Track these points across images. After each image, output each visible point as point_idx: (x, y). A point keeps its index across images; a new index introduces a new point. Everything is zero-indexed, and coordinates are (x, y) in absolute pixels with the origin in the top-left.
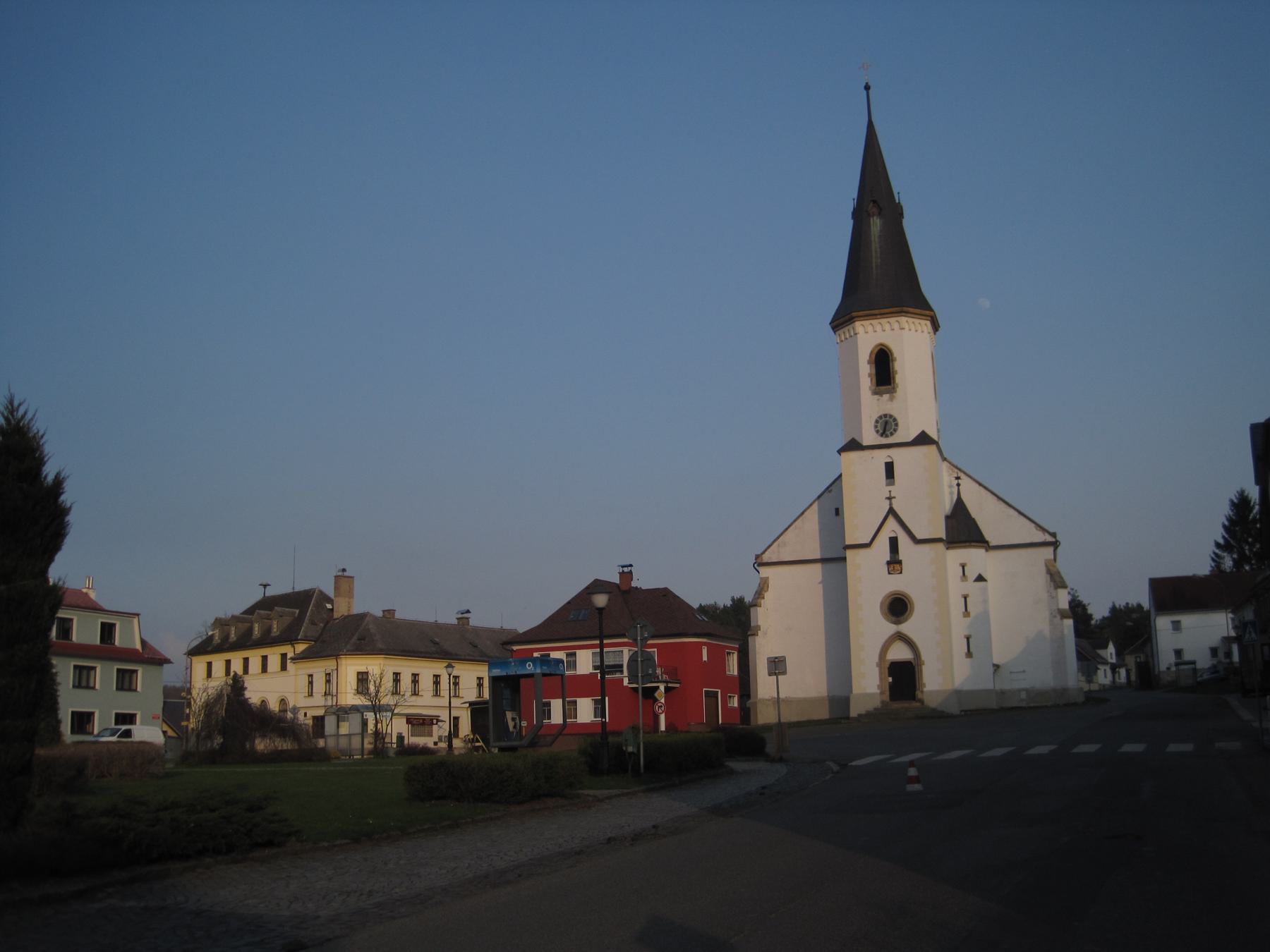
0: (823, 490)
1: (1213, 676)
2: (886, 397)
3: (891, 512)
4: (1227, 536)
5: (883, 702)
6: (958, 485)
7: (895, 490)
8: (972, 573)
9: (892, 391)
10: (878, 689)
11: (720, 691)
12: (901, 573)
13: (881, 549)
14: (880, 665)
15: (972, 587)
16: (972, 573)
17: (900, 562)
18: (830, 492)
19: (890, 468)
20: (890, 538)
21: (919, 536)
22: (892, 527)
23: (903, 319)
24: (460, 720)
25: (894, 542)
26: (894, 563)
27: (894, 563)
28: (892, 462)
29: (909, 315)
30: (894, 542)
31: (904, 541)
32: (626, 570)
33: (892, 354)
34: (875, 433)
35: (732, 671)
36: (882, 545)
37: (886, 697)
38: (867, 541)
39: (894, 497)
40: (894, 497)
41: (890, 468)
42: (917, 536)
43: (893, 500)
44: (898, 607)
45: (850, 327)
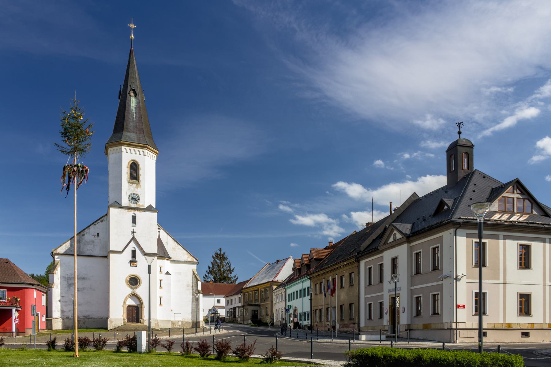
1: (396, 310)
2: (134, 185)
3: (133, 239)
6: (159, 232)
8: (164, 271)
11: (40, 313)
12: (136, 266)
13: (127, 254)
15: (163, 276)
16: (164, 271)
17: (136, 262)
20: (132, 250)
23: (146, 151)
24: (388, 292)
25: (134, 252)
26: (133, 261)
27: (133, 261)
30: (134, 252)
31: (138, 252)
36: (128, 252)
37: (126, 321)
38: (121, 250)
39: (136, 232)
40: (136, 232)
43: (135, 233)
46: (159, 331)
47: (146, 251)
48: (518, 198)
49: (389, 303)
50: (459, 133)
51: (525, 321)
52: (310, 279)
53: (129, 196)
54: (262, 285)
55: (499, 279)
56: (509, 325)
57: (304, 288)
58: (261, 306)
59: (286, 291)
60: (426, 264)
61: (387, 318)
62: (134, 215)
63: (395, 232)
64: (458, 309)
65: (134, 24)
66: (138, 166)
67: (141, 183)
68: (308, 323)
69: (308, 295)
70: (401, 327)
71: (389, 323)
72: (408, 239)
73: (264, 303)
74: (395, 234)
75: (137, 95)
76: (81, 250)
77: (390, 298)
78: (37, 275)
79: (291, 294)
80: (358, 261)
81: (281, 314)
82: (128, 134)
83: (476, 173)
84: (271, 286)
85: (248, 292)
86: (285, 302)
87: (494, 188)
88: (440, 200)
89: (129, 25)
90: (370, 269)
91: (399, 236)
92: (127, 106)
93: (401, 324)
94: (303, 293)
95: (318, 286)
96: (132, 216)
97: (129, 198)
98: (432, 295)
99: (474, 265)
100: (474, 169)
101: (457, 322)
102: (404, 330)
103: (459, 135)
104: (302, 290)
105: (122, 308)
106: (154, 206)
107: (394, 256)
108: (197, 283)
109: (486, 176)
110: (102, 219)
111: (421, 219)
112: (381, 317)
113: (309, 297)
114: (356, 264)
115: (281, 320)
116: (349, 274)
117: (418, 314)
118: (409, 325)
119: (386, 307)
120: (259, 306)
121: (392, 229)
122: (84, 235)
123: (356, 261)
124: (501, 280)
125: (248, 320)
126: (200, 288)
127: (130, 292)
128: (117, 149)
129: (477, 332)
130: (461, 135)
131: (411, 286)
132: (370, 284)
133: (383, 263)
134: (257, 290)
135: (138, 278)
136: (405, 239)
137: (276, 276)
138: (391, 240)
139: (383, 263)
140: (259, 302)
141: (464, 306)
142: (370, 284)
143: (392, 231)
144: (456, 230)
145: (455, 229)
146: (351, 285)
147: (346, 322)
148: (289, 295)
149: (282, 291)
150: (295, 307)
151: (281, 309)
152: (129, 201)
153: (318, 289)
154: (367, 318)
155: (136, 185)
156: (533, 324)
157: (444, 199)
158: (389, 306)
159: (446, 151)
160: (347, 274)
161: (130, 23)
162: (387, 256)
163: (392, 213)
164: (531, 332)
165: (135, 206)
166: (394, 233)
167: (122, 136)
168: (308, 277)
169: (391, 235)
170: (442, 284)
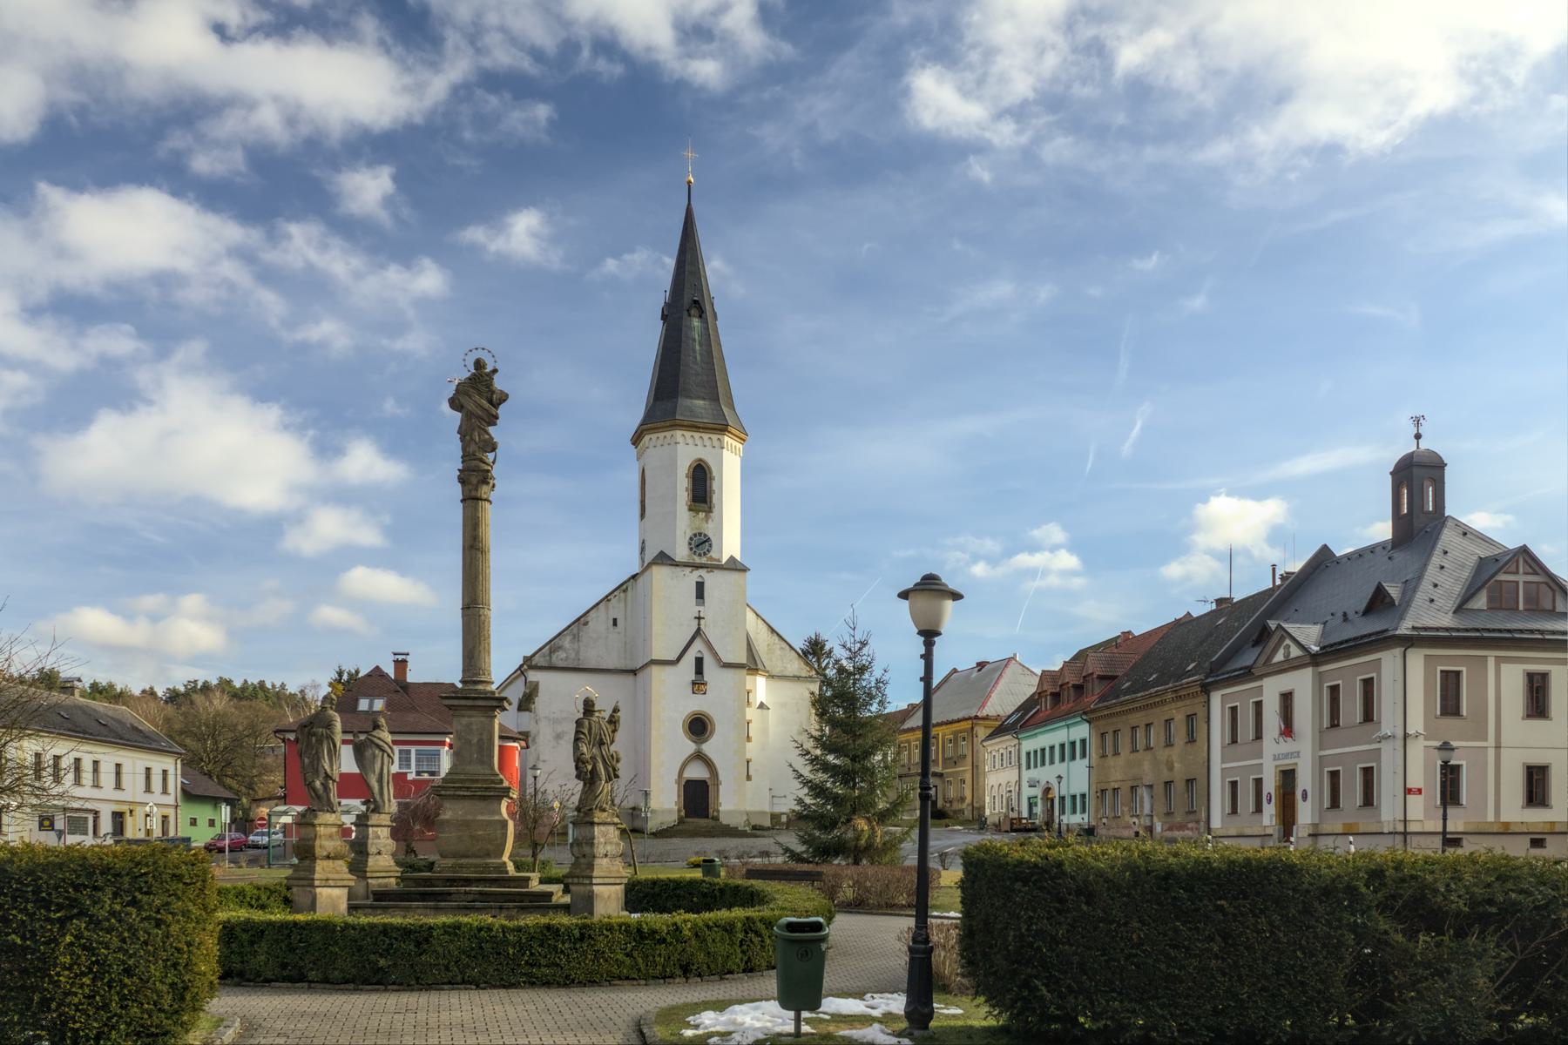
0: (601, 598)
2: (702, 515)
3: (698, 632)
4: (480, 687)
10: (676, 805)
12: (705, 693)
14: (678, 782)
18: (608, 600)
19: (700, 587)
20: (696, 658)
21: (673, 657)
25: (699, 662)
26: (698, 685)
27: (698, 685)
28: (703, 583)
29: (1477, 534)
30: (699, 662)
32: (400, 658)
33: (711, 472)
34: (688, 550)
35: (179, 762)
36: (690, 659)
37: (683, 814)
39: (703, 618)
40: (703, 618)
41: (700, 587)
42: (672, 659)
44: (699, 727)
46: (743, 834)
47: (726, 659)
48: (1525, 582)
49: (1276, 782)
50: (1418, 436)
51: (1536, 816)
52: (1089, 722)
53: (691, 539)
54: (948, 726)
55: (1486, 740)
56: (1507, 824)
57: (1072, 739)
58: (945, 775)
59: (1020, 744)
60: (1351, 708)
61: (1270, 811)
62: (700, 580)
63: (1288, 641)
64: (1408, 796)
66: (708, 472)
67: (714, 510)
68: (1083, 819)
69: (1083, 755)
70: (1300, 829)
71: (1274, 818)
72: (1314, 660)
73: (954, 770)
74: (1288, 647)
75: (703, 312)
76: (581, 658)
77: (1278, 771)
78: (273, 686)
79: (1036, 752)
80: (1206, 689)
81: (1004, 797)
82: (688, 402)
83: (1449, 524)
84: (972, 728)
85: (908, 742)
86: (1017, 770)
87: (1482, 556)
88: (1376, 583)
90: (1234, 710)
91: (1295, 652)
92: (683, 339)
93: (1299, 822)
94: (1069, 752)
95: (1109, 738)
96: (697, 583)
97: (690, 544)
98: (1360, 768)
99: (1439, 713)
100: (1446, 515)
101: (1408, 819)
102: (1306, 835)
103: (1420, 431)
104: (1066, 746)
105: (676, 786)
107: (1285, 688)
109: (1469, 530)
110: (624, 587)
111: (1339, 615)
112: (1259, 809)
113: (1086, 762)
114: (1202, 698)
115: (1004, 810)
116: (1184, 718)
117: (1335, 803)
118: (1315, 825)
119: (1270, 786)
121: (1282, 635)
122: (586, 624)
123: (1201, 691)
124: (1491, 741)
125: (915, 810)
127: (692, 752)
128: (665, 437)
129: (1441, 837)
130: (1420, 441)
131: (1320, 750)
132: (1234, 741)
133: (1261, 701)
135: (708, 719)
136: (1308, 660)
137: (983, 705)
138: (1279, 657)
139: (1261, 701)
140: (938, 766)
141: (1419, 791)
142: (1234, 741)
143: (1282, 639)
144: (1405, 650)
145: (1403, 649)
146: (1191, 739)
147: (1178, 819)
148: (1028, 754)
149: (1008, 743)
150: (1048, 782)
151: (1004, 787)
152: (691, 549)
153: (1108, 744)
154: (1228, 810)
155: (704, 514)
156: (1552, 823)
157: (1384, 584)
158: (1276, 786)
159: (1391, 473)
160: (1179, 718)
162: (1271, 689)
163: (1277, 584)
164: (1549, 839)
165: (704, 560)
166: (1285, 644)
167: (676, 407)
168: (1085, 717)
169: (1280, 647)
170: (1380, 749)
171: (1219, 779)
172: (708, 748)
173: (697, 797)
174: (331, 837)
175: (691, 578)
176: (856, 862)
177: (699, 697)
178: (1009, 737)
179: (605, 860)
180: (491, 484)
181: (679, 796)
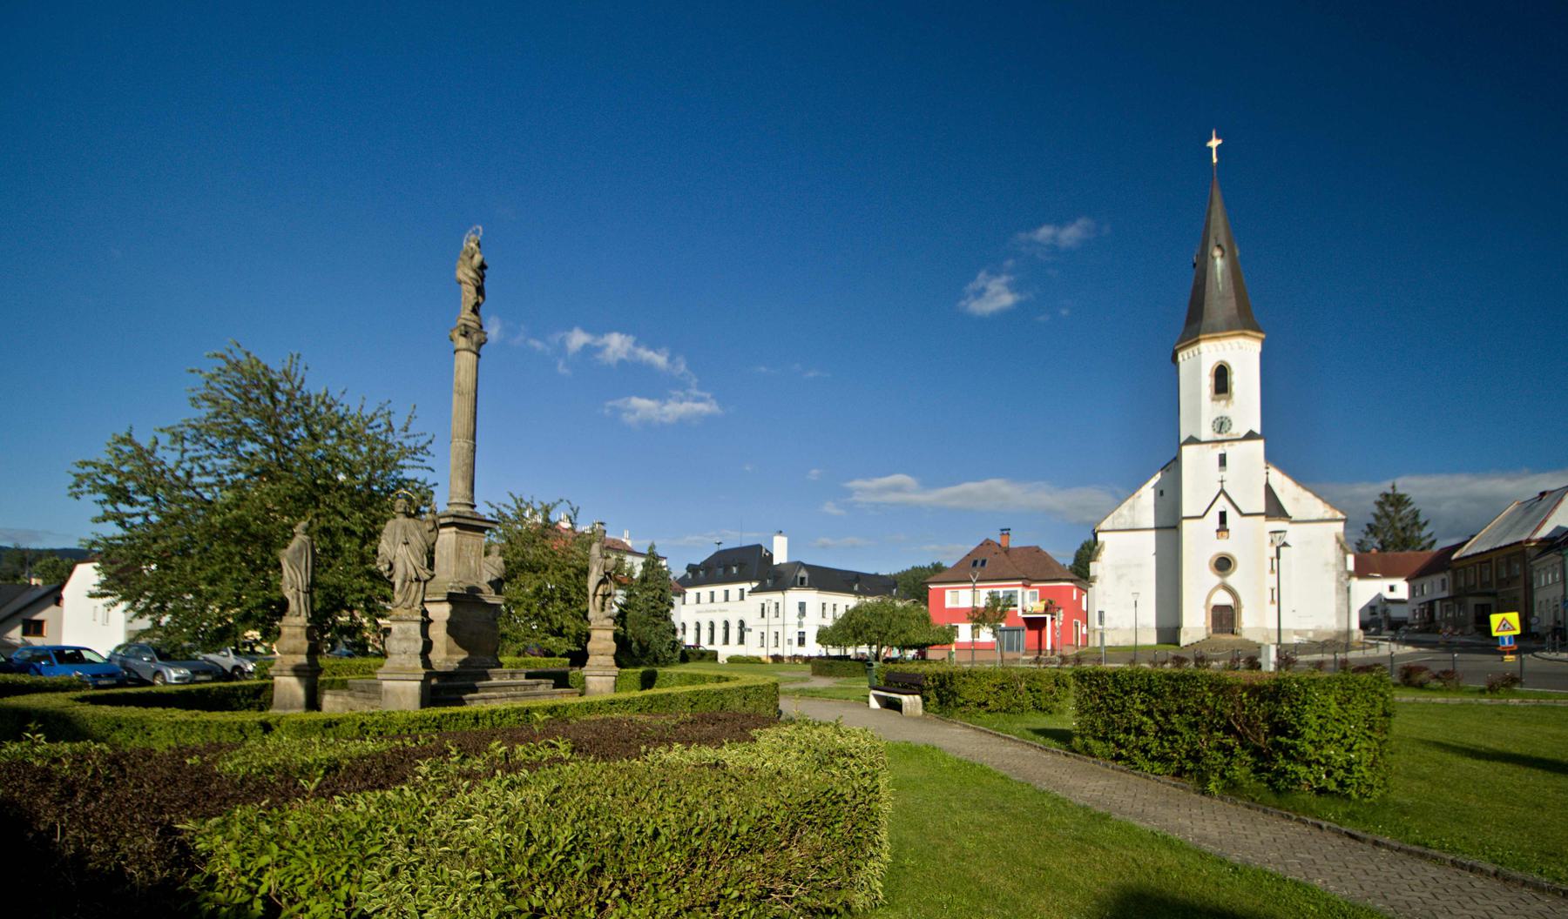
2: (1223, 403)
3: (1222, 491)
5: (1207, 634)
7: (1226, 475)
9: (1230, 397)
22: (1222, 504)
25: (1223, 516)
30: (1223, 516)
31: (1232, 516)
36: (1213, 518)
37: (1210, 631)
38: (1201, 514)
44: (1223, 564)
45: (1195, 348)
55: (1004, 592)
60: (1196, 352)
65: (1218, 137)
85: (1464, 567)
89: (1214, 133)
106: (1258, 430)
108: (1345, 559)
120: (1494, 594)
126: (1351, 566)
134: (1489, 561)
161: (1210, 139)
171: (1430, 639)
172: (1231, 580)
173: (1224, 618)
174: (295, 636)
175: (1214, 453)
176: (568, 765)
177: (1224, 414)
178: (1552, 555)
179: (403, 656)
180: (174, 446)
181: (1207, 618)
